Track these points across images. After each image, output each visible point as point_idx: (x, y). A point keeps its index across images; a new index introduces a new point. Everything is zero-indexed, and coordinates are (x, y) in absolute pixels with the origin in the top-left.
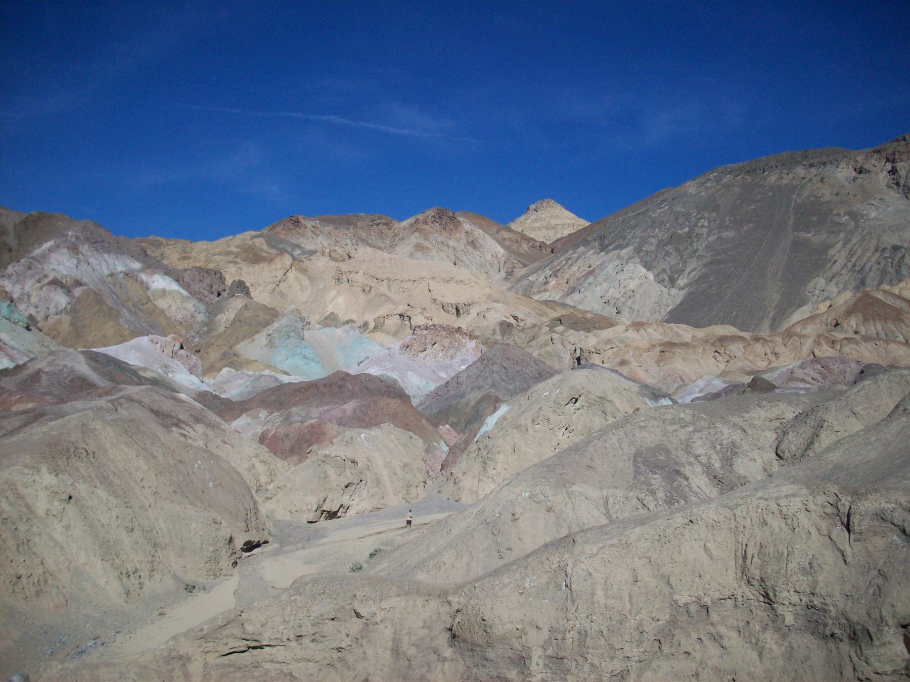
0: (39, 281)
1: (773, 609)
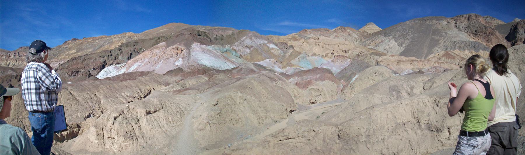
0: (243, 46)
1: (420, 124)
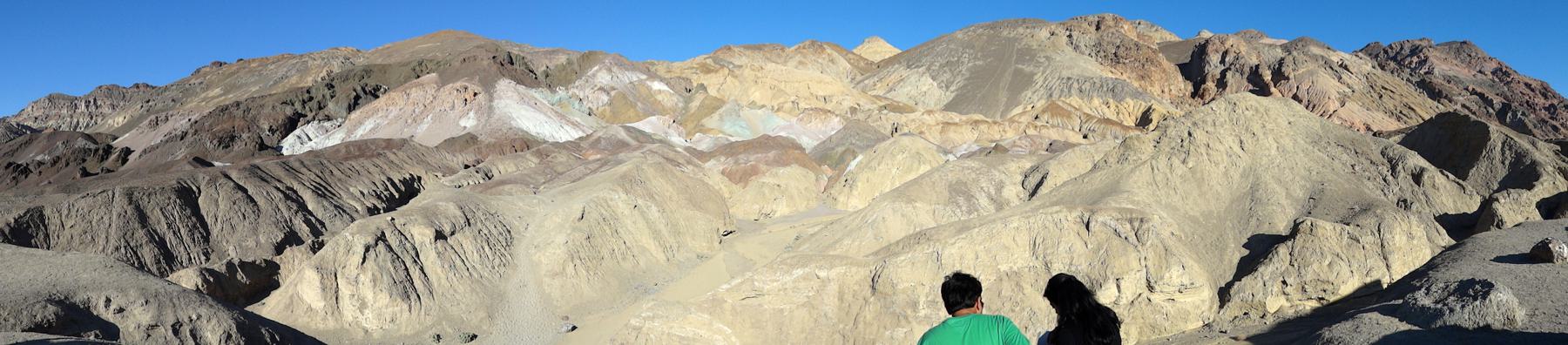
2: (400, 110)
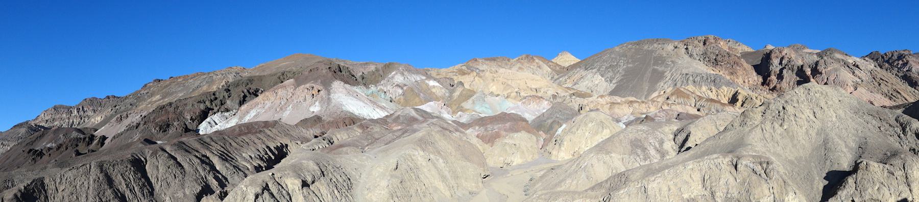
0: (392, 85)
2: (272, 103)
